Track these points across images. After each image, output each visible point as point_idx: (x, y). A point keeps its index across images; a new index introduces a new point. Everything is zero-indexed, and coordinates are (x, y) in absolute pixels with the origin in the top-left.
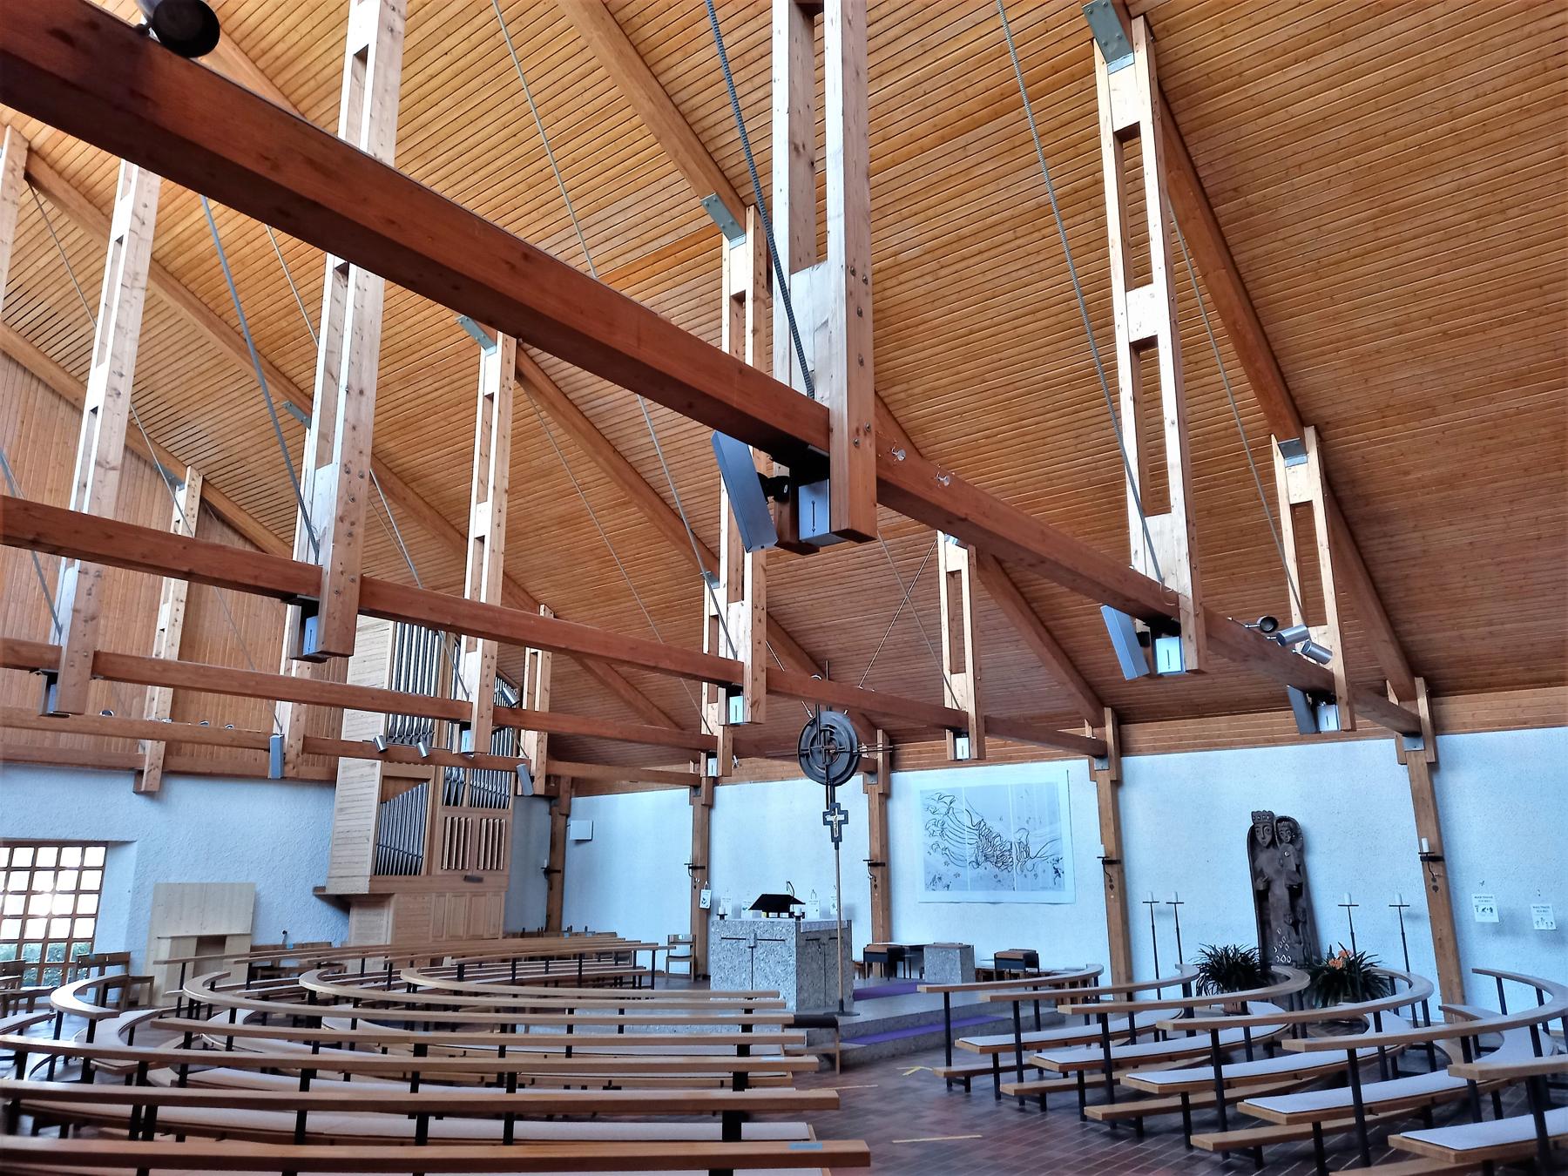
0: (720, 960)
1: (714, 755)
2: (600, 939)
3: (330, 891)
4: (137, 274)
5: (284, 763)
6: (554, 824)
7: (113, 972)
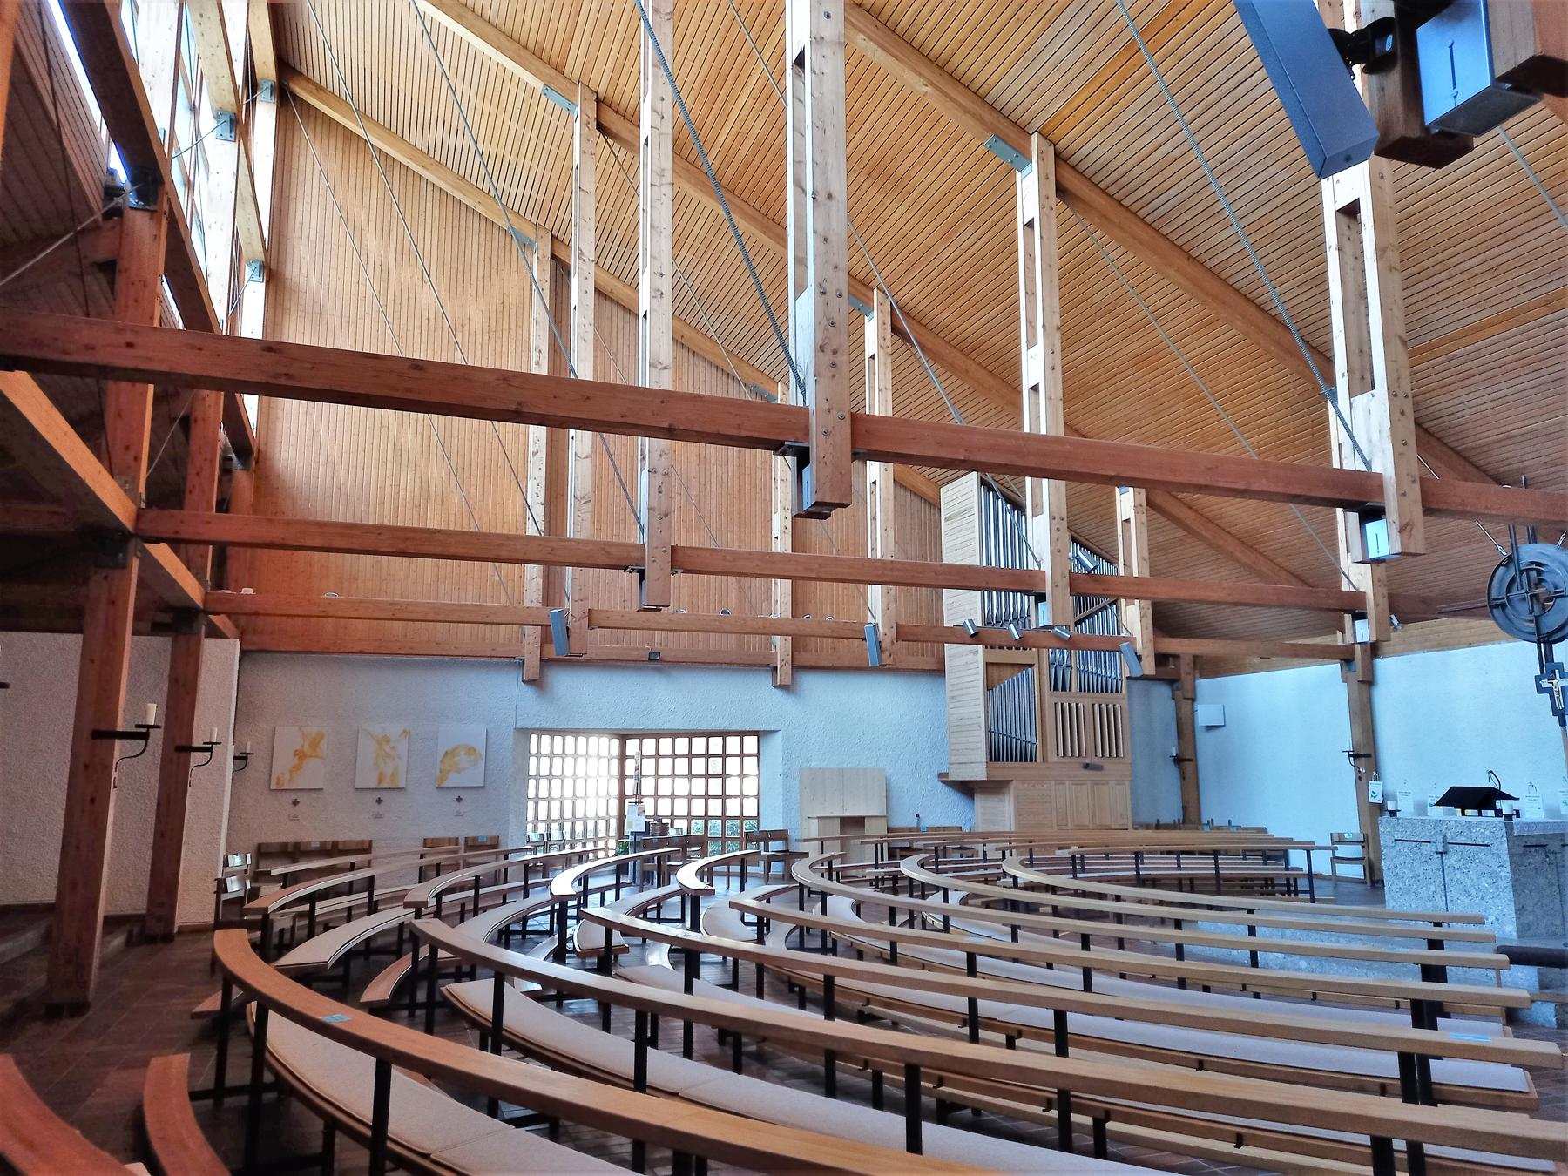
0: (1396, 867)
1: (1362, 616)
2: (1243, 834)
3: (952, 777)
4: (663, 170)
5: (881, 650)
6: (1178, 709)
7: (776, 846)
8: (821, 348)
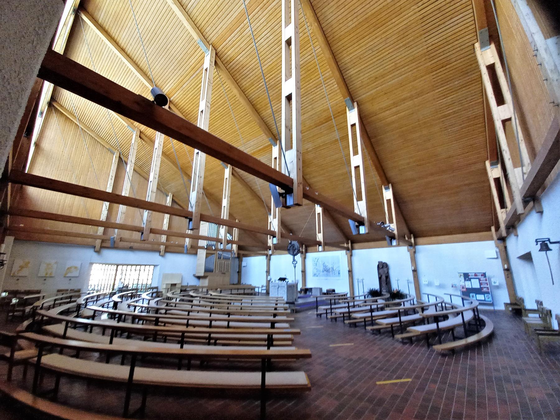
7: (155, 290)
8: (196, 202)
